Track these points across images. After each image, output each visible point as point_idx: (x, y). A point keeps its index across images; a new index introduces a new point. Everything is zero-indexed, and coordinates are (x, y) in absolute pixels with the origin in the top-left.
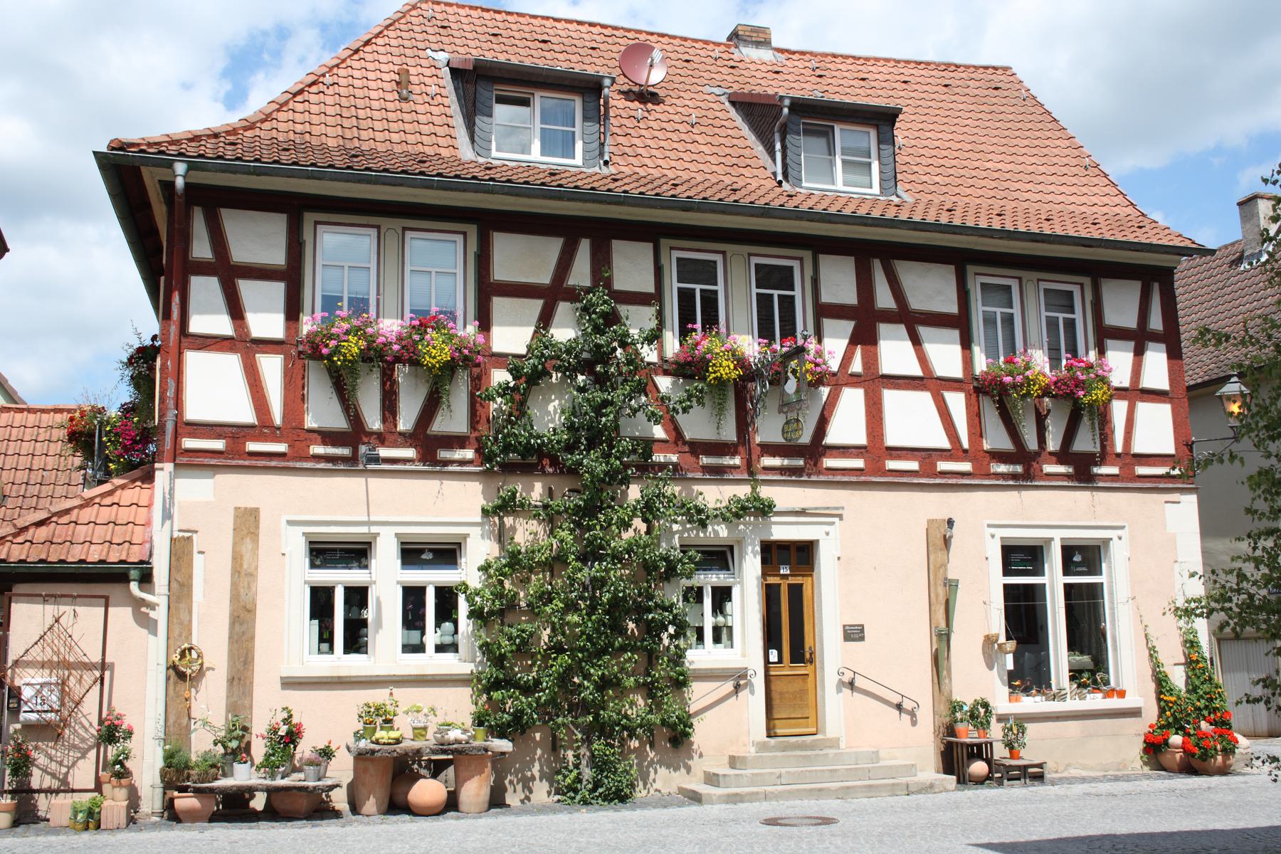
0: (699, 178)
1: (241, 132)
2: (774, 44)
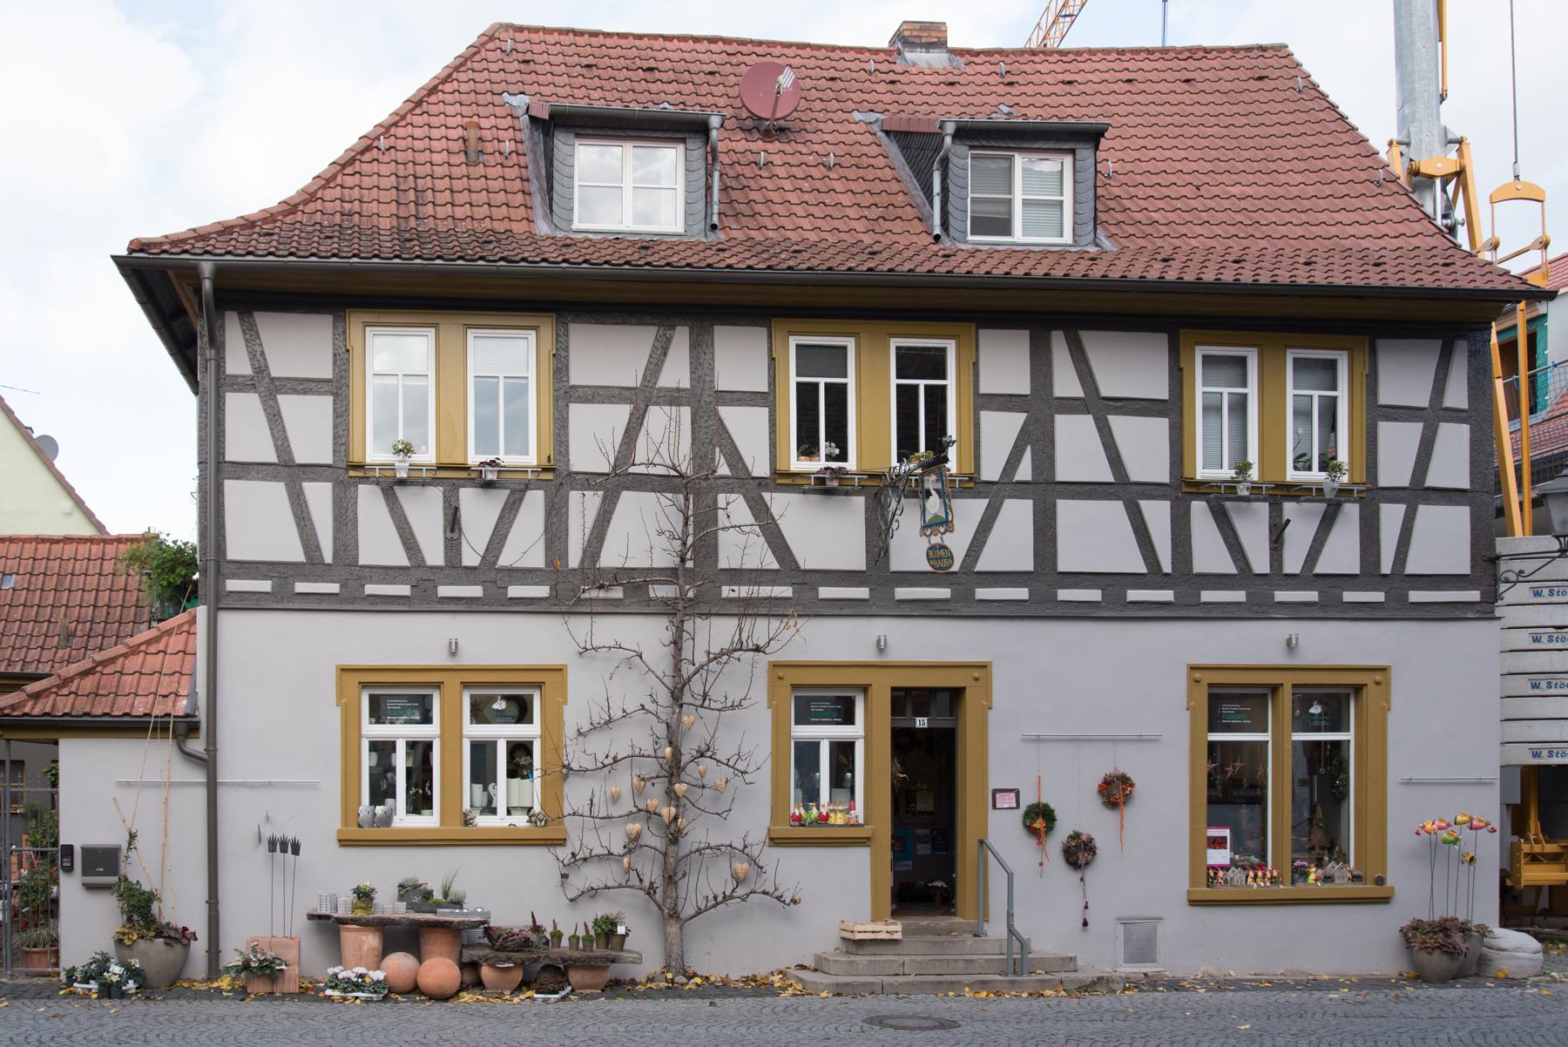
0: (831, 238)
1: (280, 218)
2: (951, 44)
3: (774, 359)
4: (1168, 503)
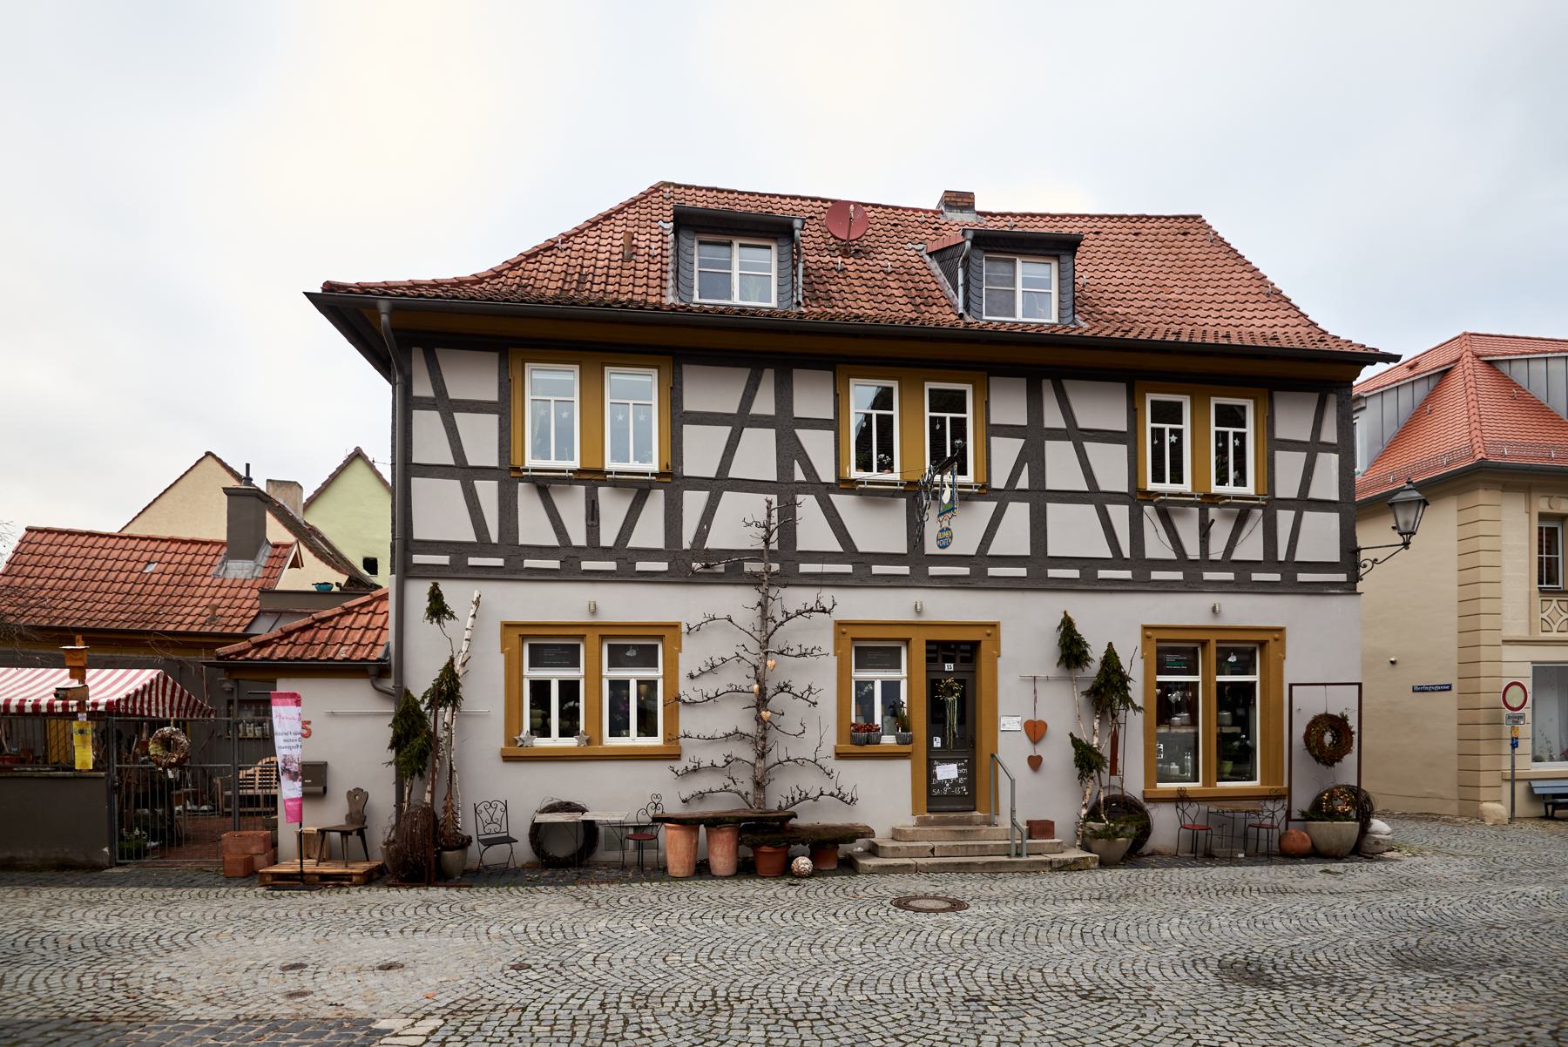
2: (978, 208)
3: (838, 395)
4: (1127, 507)
